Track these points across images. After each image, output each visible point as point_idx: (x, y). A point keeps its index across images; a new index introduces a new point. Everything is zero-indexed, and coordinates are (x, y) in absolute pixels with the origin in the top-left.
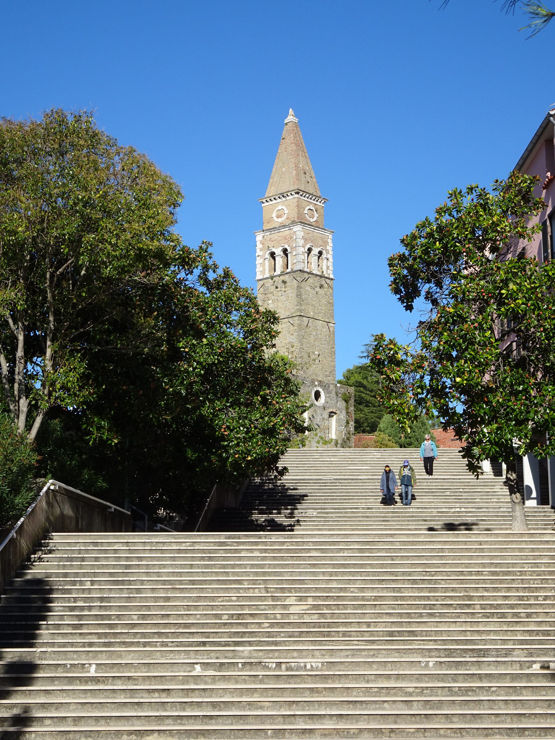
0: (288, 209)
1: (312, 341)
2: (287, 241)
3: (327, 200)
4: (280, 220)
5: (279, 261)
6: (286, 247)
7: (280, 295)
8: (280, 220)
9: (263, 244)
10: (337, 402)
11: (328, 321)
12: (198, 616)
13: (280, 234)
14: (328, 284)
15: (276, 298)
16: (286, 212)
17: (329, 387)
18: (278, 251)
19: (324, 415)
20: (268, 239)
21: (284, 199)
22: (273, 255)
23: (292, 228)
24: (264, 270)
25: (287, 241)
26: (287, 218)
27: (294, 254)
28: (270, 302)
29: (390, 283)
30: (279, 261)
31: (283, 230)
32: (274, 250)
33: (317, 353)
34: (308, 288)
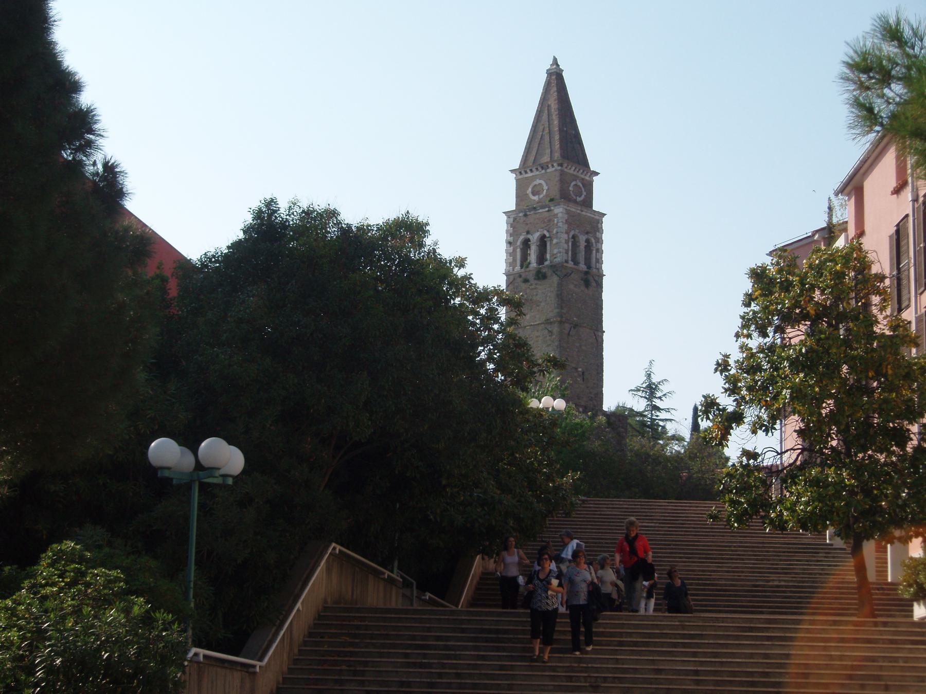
16: (545, 187)
34: (572, 287)
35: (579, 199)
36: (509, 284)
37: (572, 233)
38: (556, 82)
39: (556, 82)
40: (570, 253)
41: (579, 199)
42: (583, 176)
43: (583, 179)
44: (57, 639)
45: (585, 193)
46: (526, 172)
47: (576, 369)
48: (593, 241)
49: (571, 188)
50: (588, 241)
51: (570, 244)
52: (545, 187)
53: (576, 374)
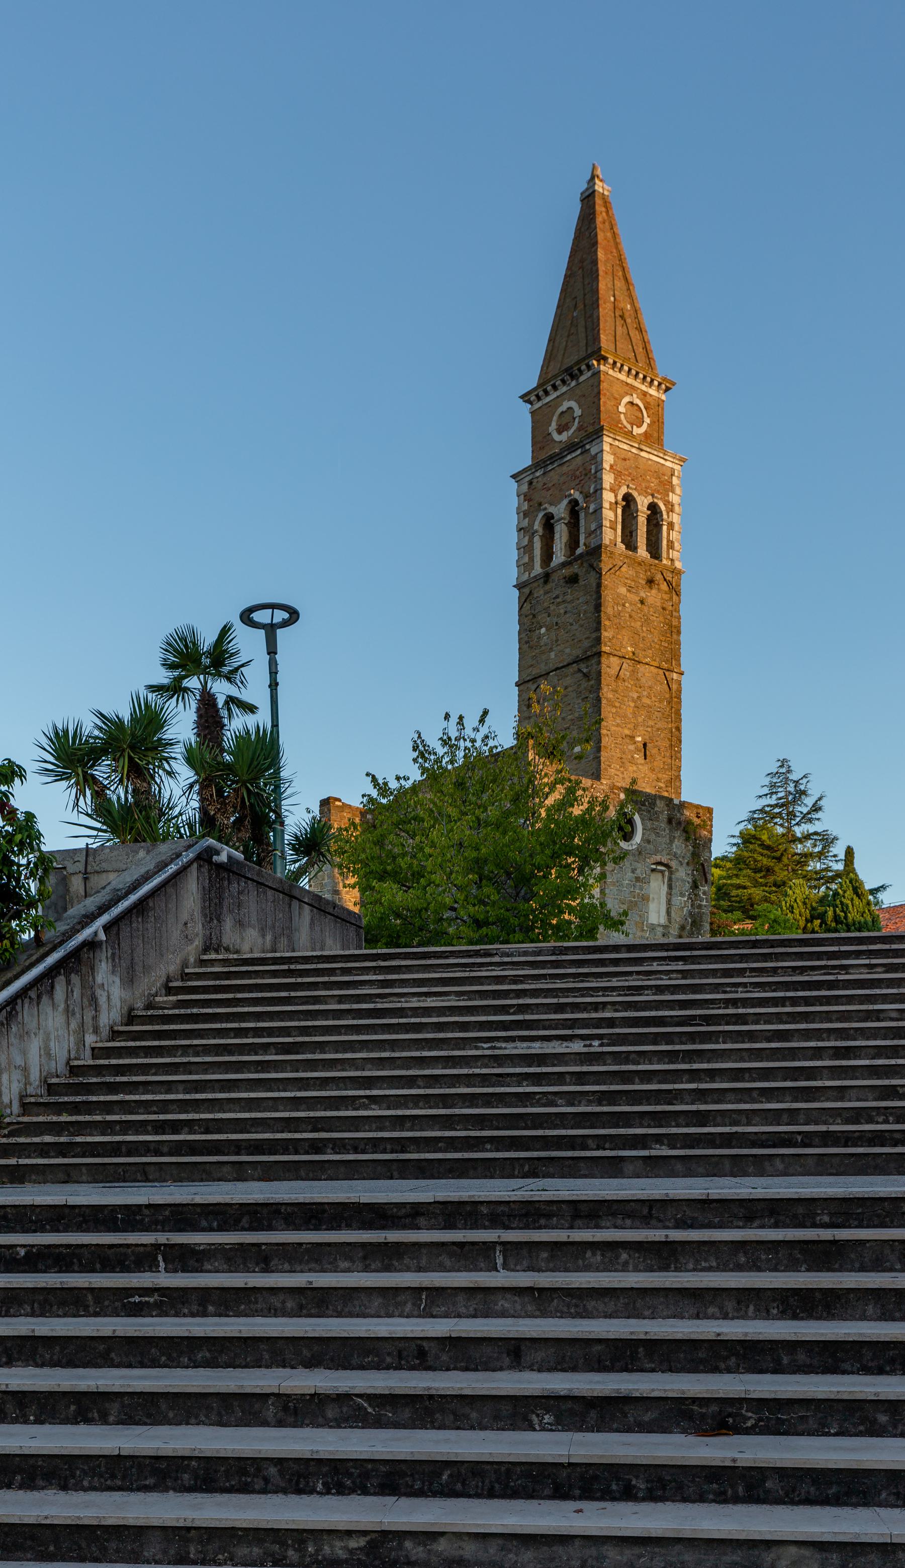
0: (580, 407)
1: (629, 711)
2: (577, 481)
3: (674, 384)
4: (564, 437)
5: (561, 534)
6: (577, 495)
7: (562, 611)
8: (564, 437)
9: (529, 500)
10: (671, 842)
11: (665, 666)
12: (778, 1162)
13: (565, 469)
14: (669, 583)
15: (555, 620)
16: (578, 412)
17: (653, 804)
18: (560, 510)
19: (638, 871)
20: (540, 485)
21: (573, 383)
22: (549, 523)
23: (588, 447)
24: (532, 559)
25: (577, 481)
26: (580, 429)
27: (591, 510)
28: (543, 630)
29: (816, 822)
30: (561, 534)
31: (569, 457)
32: (552, 509)
33: (639, 739)
34: (623, 590)
35: (637, 431)
36: (133, 718)
37: (623, 490)
38: (589, 198)
39: (589, 198)
40: (619, 527)
41: (637, 431)
42: (644, 388)
43: (645, 394)
44: (209, 734)
45: (647, 421)
46: (547, 393)
47: (632, 738)
48: (663, 508)
49: (622, 409)
50: (653, 507)
51: (619, 511)
52: (578, 412)
53: (632, 747)
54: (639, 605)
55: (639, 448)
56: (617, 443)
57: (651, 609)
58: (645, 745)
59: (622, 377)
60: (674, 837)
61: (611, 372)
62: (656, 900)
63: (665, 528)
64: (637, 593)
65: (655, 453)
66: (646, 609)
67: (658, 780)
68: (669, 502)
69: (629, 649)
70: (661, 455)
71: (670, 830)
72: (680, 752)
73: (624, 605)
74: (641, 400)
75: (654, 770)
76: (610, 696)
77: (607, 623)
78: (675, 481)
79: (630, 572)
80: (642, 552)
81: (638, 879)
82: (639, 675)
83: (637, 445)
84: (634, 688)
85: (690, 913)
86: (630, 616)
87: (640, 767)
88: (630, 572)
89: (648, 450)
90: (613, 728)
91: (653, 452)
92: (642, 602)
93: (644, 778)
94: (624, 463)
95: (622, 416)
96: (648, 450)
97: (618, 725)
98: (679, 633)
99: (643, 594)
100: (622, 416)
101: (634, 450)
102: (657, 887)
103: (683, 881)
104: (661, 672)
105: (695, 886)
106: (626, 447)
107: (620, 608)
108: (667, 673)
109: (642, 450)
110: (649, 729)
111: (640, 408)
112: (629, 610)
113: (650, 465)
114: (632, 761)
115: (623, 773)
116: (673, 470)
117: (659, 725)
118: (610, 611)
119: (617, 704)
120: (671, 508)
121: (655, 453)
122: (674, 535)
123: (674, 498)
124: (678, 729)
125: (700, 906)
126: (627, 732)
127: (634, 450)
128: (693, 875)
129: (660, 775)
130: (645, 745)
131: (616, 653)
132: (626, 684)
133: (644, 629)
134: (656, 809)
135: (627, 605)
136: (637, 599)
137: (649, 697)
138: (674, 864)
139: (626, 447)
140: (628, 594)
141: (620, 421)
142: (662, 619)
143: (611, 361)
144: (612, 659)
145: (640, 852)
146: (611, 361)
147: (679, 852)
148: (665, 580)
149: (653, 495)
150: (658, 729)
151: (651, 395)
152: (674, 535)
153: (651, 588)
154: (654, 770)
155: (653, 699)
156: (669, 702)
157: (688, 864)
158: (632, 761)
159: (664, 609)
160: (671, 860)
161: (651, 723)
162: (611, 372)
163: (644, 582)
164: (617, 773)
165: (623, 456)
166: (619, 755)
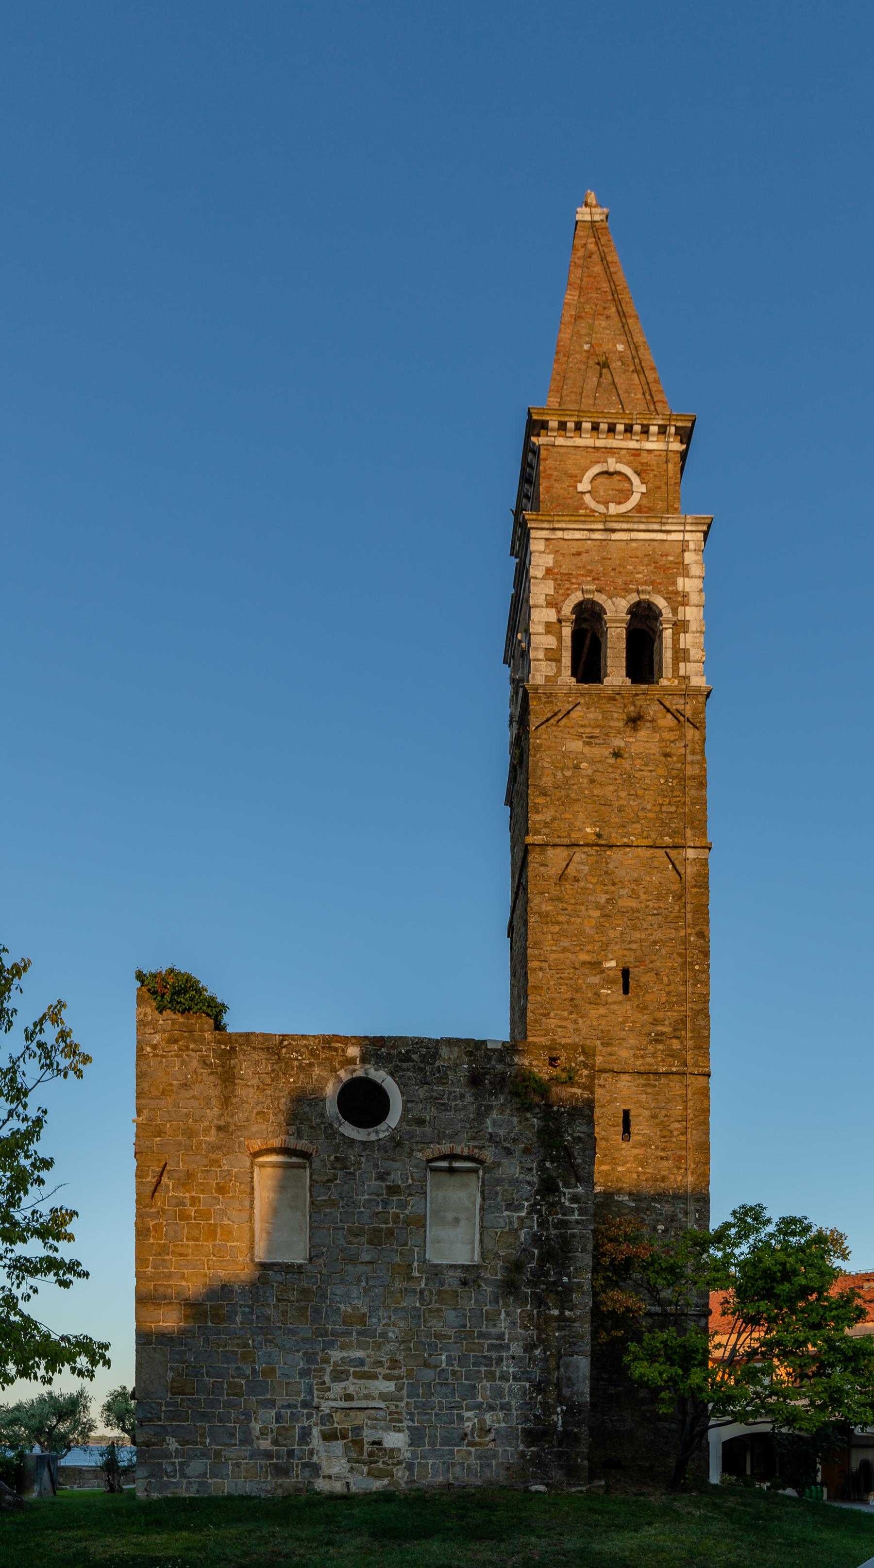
34: (576, 745)
42: (633, 445)
47: (595, 966)
53: (595, 980)
54: (612, 761)
55: (606, 530)
56: (559, 534)
57: (638, 761)
58: (626, 973)
59: (586, 440)
60: (489, 1108)
61: (560, 441)
62: (463, 1223)
63: (668, 634)
64: (605, 744)
65: (642, 527)
66: (626, 764)
67: (656, 1022)
68: (677, 593)
69: (588, 830)
70: (656, 527)
71: (476, 1097)
72: (706, 971)
73: (577, 767)
74: (628, 464)
75: (646, 1008)
76: (546, 907)
77: (541, 800)
78: (689, 558)
79: (590, 716)
80: (616, 675)
81: (393, 1190)
82: (611, 866)
83: (600, 526)
84: (599, 888)
85: (536, 1240)
86: (592, 781)
87: (614, 1007)
88: (590, 716)
89: (625, 526)
90: (553, 956)
91: (636, 526)
92: (617, 755)
93: (624, 1022)
94: (576, 560)
95: (587, 498)
96: (625, 526)
97: (564, 950)
98: (702, 785)
99: (618, 742)
100: (587, 498)
101: (597, 536)
102: (461, 1196)
103: (514, 1182)
104: (660, 853)
105: (548, 1188)
106: (578, 535)
107: (568, 773)
108: (673, 853)
109: (614, 531)
110: (634, 946)
111: (626, 476)
112: (590, 772)
113: (636, 549)
114: (596, 1000)
115: (575, 1022)
116: (685, 542)
117: (658, 935)
118: (547, 781)
119: (561, 918)
120: (679, 600)
121: (642, 527)
122: (687, 640)
123: (689, 585)
124: (702, 935)
125: (563, 1224)
126: (584, 957)
127: (597, 536)
128: (542, 1168)
129: (660, 1015)
130: (626, 973)
131: (558, 841)
132: (582, 884)
133: (623, 794)
134: (438, 1063)
135: (584, 765)
136: (606, 752)
137: (634, 895)
138: (489, 1155)
139: (578, 535)
140: (586, 749)
141: (582, 505)
142: (662, 771)
143: (553, 424)
144: (550, 852)
145: (396, 1143)
146: (553, 424)
147: (502, 1132)
148: (668, 711)
149: (638, 592)
150: (655, 943)
151: (649, 451)
152: (687, 640)
153: (635, 729)
154: (646, 1008)
155: (643, 897)
156: (679, 897)
157: (526, 1151)
158: (596, 1000)
159: (666, 755)
160: (481, 1148)
161: (637, 935)
162: (560, 441)
163: (621, 724)
164: (563, 1023)
165: (574, 551)
166: (569, 995)
